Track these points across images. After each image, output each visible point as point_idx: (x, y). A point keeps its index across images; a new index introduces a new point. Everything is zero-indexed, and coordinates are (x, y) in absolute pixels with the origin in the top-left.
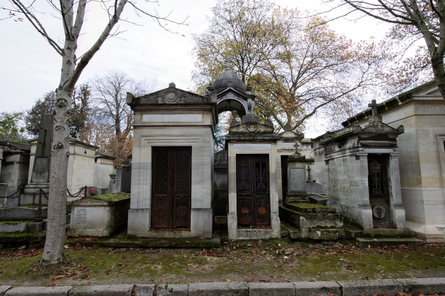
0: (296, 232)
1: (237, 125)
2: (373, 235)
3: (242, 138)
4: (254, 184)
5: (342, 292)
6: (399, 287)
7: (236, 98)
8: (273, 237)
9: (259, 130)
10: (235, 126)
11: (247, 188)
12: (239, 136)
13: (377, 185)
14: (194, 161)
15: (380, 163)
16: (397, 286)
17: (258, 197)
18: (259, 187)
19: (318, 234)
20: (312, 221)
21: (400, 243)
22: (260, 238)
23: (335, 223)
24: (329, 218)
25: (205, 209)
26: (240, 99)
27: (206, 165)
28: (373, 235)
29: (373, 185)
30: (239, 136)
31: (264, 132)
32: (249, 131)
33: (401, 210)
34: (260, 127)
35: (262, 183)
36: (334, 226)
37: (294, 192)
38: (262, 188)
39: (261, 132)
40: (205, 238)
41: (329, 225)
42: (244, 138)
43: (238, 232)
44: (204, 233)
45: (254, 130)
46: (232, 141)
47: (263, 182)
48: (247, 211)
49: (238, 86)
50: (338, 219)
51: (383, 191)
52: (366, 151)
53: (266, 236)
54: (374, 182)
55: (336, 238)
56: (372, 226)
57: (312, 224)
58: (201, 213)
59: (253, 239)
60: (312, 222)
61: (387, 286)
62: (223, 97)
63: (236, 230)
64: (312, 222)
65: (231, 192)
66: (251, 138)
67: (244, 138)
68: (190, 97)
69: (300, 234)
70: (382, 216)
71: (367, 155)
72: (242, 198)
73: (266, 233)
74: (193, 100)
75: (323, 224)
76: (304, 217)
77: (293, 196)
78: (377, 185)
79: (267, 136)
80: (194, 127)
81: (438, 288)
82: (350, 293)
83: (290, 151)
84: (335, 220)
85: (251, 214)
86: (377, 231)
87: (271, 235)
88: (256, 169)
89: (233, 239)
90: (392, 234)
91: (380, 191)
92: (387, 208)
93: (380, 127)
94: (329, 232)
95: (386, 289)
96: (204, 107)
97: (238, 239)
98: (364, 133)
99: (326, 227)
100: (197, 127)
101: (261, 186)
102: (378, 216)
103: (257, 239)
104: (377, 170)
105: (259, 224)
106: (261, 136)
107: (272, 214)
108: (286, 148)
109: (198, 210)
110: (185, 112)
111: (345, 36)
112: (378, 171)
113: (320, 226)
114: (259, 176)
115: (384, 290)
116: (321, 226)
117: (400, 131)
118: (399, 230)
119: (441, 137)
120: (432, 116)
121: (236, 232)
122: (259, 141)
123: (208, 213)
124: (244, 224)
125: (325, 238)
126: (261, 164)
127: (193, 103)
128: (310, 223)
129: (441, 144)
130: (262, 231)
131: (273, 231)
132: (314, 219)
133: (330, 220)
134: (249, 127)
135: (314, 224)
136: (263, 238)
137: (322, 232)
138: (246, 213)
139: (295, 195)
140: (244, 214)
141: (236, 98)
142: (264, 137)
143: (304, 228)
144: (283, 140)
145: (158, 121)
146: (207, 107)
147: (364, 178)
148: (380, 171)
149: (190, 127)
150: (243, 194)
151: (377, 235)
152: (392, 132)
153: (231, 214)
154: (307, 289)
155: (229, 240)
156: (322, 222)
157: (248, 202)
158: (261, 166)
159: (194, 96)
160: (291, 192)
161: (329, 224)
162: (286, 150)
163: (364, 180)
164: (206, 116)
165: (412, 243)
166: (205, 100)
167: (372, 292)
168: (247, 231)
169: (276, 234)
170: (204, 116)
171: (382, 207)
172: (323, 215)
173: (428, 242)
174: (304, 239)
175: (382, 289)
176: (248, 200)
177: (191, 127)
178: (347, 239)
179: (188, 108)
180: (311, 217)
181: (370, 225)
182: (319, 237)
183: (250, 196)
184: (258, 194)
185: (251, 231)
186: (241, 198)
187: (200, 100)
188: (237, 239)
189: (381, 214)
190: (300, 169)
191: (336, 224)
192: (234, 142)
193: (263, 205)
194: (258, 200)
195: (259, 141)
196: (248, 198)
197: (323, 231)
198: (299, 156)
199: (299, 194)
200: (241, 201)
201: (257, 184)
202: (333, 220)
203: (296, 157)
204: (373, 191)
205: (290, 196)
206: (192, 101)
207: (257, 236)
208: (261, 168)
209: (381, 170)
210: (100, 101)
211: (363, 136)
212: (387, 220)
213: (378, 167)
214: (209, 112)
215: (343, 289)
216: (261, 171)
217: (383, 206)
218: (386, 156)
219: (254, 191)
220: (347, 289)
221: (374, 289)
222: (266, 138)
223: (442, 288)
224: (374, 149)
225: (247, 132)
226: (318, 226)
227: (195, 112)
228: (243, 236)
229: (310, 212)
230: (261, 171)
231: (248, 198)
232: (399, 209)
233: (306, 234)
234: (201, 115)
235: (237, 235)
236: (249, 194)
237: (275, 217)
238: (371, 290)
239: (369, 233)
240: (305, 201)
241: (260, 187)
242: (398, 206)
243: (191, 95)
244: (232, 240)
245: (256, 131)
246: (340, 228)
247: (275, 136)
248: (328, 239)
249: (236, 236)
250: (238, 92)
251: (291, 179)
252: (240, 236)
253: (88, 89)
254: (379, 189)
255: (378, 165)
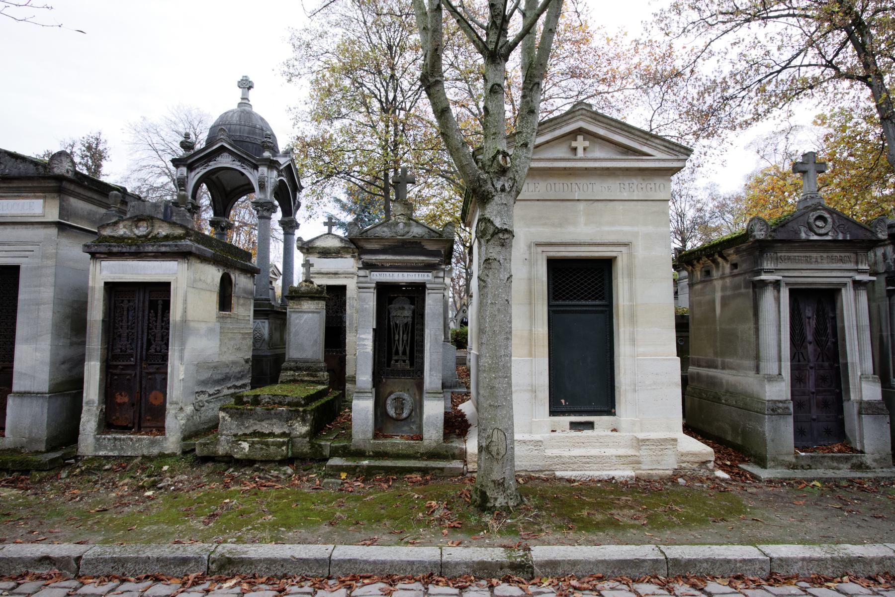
0: (208, 444)
1: (113, 221)
2: (371, 453)
3: (115, 250)
4: (142, 344)
5: (79, 568)
6: (198, 562)
7: (237, 166)
8: (166, 452)
9: (155, 232)
10: (108, 225)
11: (129, 351)
12: (110, 246)
13: (401, 349)
14: (24, 295)
15: (412, 303)
16: (195, 558)
17: (151, 370)
18: (152, 351)
19: (244, 448)
20: (243, 422)
21: (411, 470)
22: (139, 453)
23: (291, 426)
24: (279, 416)
25: (38, 393)
26: (246, 167)
27: (44, 304)
28: (371, 453)
29: (394, 350)
30: (110, 246)
31: (167, 237)
32: (135, 234)
33: (436, 402)
34: (160, 227)
35: (126, 342)
36: (287, 432)
37: (296, 361)
38: (160, 352)
39: (160, 236)
40: (33, 451)
41: (277, 431)
42: (120, 249)
43: (98, 440)
44: (31, 440)
45: (144, 233)
46: (97, 255)
47: (128, 341)
48: (126, 399)
49: (248, 140)
50: (299, 419)
51: (412, 364)
52: (374, 278)
53: (151, 450)
54: (397, 342)
55: (279, 458)
56: (370, 435)
57: (242, 427)
58: (26, 401)
59: (125, 455)
60: (243, 425)
61: (175, 558)
62: (211, 163)
63: (95, 435)
64: (243, 425)
65: (89, 360)
66: (133, 249)
67: (120, 249)
68: (11, 162)
69: (215, 447)
70: (404, 415)
71: (374, 285)
72: (118, 371)
73: (153, 443)
74: (16, 170)
75: (264, 427)
76: (227, 413)
77: (291, 369)
78: (401, 349)
79: (165, 246)
80: (24, 226)
81: (282, 566)
82: (94, 571)
83: (331, 275)
84: (291, 420)
85: (133, 405)
86: (379, 444)
87: (162, 448)
88: (150, 312)
89: (87, 454)
90: (411, 451)
91: (407, 362)
92: (417, 397)
93: (401, 225)
94: (267, 444)
95: (170, 564)
96: (43, 185)
97: (97, 454)
98: (368, 240)
99: (271, 434)
100: (31, 226)
101: (158, 349)
102: (396, 414)
103: (133, 455)
104: (404, 317)
105: (148, 424)
106: (153, 246)
107: (168, 405)
108: (323, 271)
109: (22, 394)
110: (9, 194)
111: (625, 30)
112: (405, 321)
113: (258, 432)
114: (156, 328)
115: (167, 565)
116: (261, 431)
117: (444, 235)
118: (426, 442)
119: (540, 249)
120: (529, 203)
121: (94, 441)
122: (153, 254)
123: (41, 401)
124: (119, 423)
125: (258, 456)
126: (160, 302)
127: (16, 175)
128: (237, 425)
129: (539, 262)
130: (144, 439)
131: (166, 439)
132: (248, 418)
133: (280, 420)
134: (137, 227)
135: (246, 428)
136: (145, 454)
137: (252, 445)
138: (124, 403)
139: (297, 367)
140: (119, 404)
141: (237, 166)
142: (160, 246)
143: (224, 435)
144: (319, 253)
145: (27, 212)
146: (50, 185)
147: (364, 334)
148: (410, 319)
149: (16, 227)
150: (120, 363)
151: (380, 452)
152: (427, 236)
153: (87, 403)
154: (8, 559)
155: (79, 456)
156: (263, 423)
157: (128, 379)
158: (160, 307)
159: (19, 161)
160: (289, 361)
161: (277, 428)
162: (323, 274)
163: (364, 339)
164: (49, 201)
165: (437, 471)
166: (41, 170)
167: (139, 569)
168: (115, 439)
169: (172, 446)
170: (47, 204)
171: (406, 396)
172: (268, 409)
173: (471, 470)
174: (222, 457)
175: (161, 564)
176: (128, 377)
177: (19, 226)
178: (312, 460)
179: (11, 185)
180: (242, 414)
181: (364, 432)
182: (245, 454)
183: (134, 367)
184: (149, 364)
185: (124, 440)
186: (115, 371)
187: (31, 170)
188: (94, 454)
189: (402, 409)
190: (310, 315)
191: (293, 429)
192: (102, 256)
193: (159, 387)
194: (150, 377)
195: (153, 254)
196: (129, 372)
197: (253, 441)
198: (308, 286)
199: (305, 365)
200: (116, 377)
201: (149, 344)
202: (287, 421)
203: (303, 289)
204: (393, 362)
205: (286, 369)
206: (15, 172)
207: (135, 449)
208: (160, 312)
209: (413, 318)
210: (159, 171)
211: (369, 246)
212: (414, 422)
213: (406, 312)
214: (55, 195)
215: (82, 562)
216: (159, 317)
217: (409, 394)
218: (419, 289)
219: (141, 359)
220: (89, 562)
221: (145, 562)
222: (163, 249)
223: (289, 566)
224: (391, 273)
225: (132, 236)
226: (255, 431)
227: (29, 194)
228: (107, 449)
229: (248, 402)
230: (159, 317)
231: (129, 372)
232: (431, 400)
233: (228, 448)
234: (41, 201)
235: (95, 447)
236: (131, 365)
237: (174, 412)
238: (139, 564)
239: (362, 447)
240: (315, 379)
241: (156, 349)
242: (434, 394)
243: (13, 160)
244: (84, 456)
245: (149, 234)
246: (299, 437)
247: (182, 245)
248: (264, 459)
249: (93, 448)
250: (239, 153)
251: (292, 335)
252: (100, 450)
253: (101, 148)
254: (405, 358)
255: (407, 306)
